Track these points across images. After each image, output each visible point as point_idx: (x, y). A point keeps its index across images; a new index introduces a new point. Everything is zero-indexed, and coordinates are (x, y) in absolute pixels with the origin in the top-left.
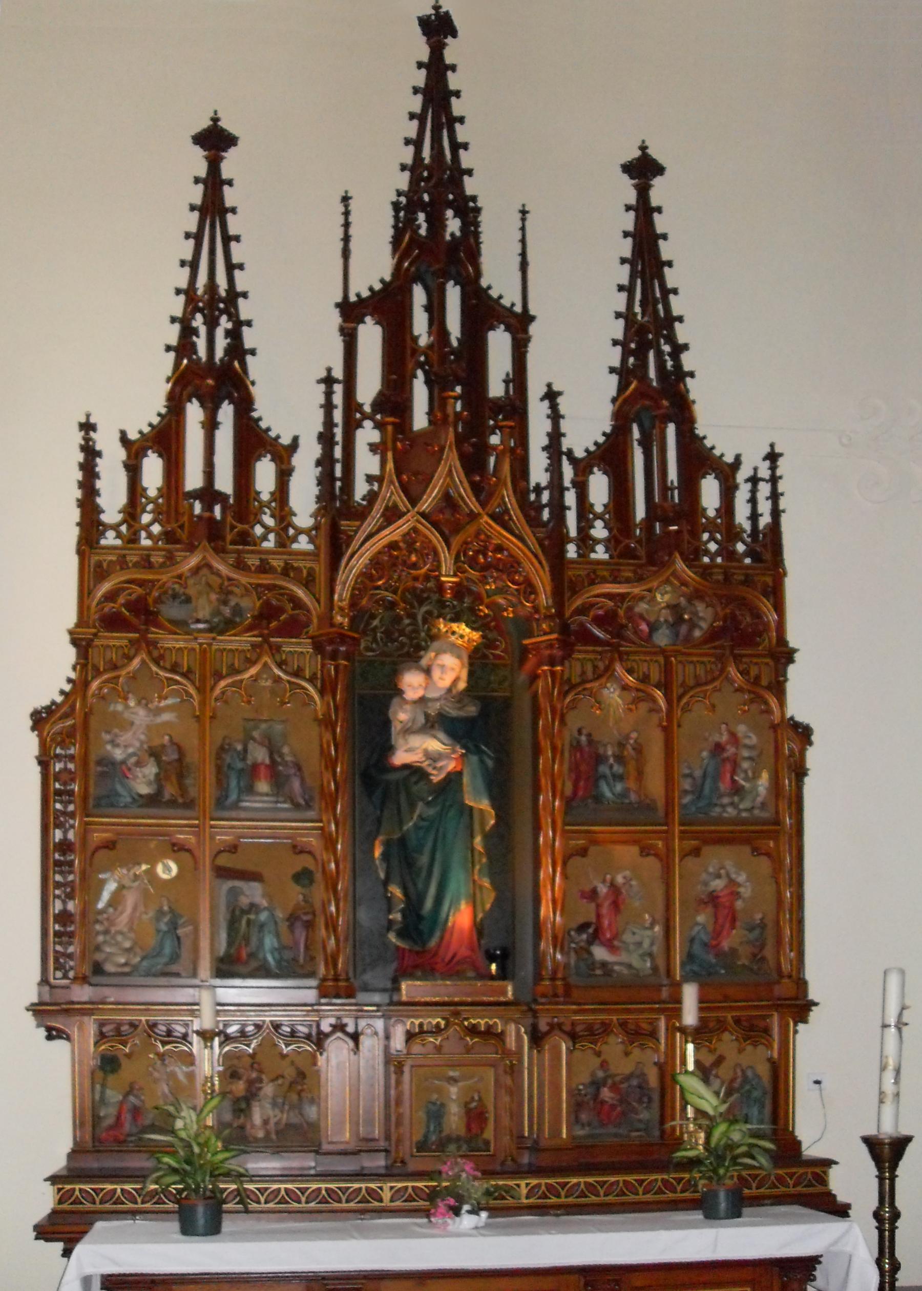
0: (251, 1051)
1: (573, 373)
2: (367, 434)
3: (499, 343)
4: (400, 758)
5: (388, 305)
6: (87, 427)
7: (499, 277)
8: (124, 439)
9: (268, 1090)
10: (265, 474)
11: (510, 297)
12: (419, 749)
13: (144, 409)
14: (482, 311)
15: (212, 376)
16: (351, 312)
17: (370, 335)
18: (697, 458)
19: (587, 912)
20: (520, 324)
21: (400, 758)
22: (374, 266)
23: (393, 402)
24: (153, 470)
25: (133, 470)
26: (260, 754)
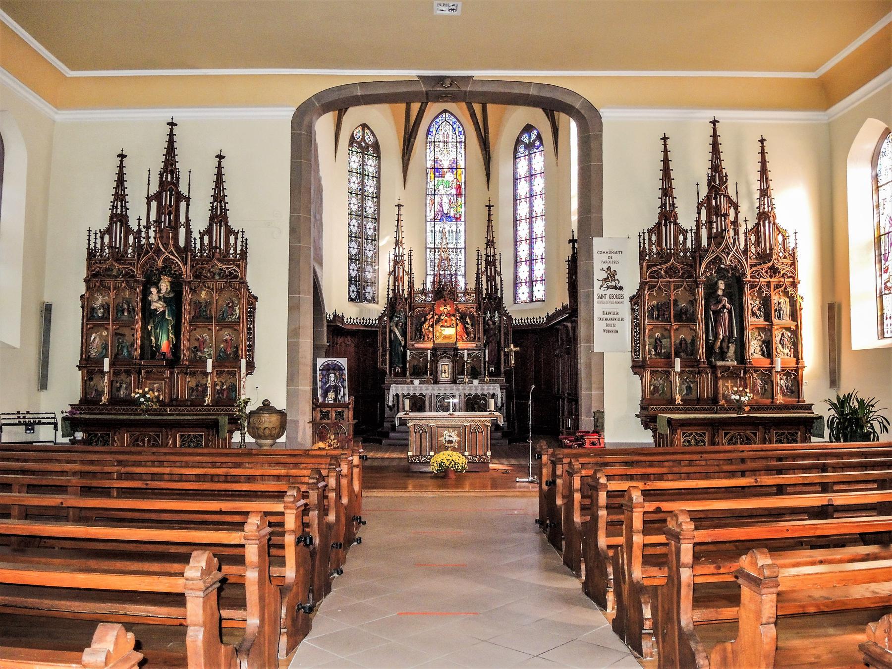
0: (496, 389)
1: (198, 215)
2: (153, 228)
3: (183, 204)
4: (152, 308)
5: (158, 197)
6: (90, 231)
7: (183, 189)
8: (200, 232)
9: (124, 386)
10: (232, 239)
11: (186, 193)
12: (158, 306)
13: (104, 224)
14: (179, 197)
15: (667, 215)
16: (149, 200)
17: (154, 204)
18: (229, 231)
19: (197, 344)
20: (188, 199)
21: (152, 308)
22: (154, 189)
23: (158, 222)
24: (206, 239)
25: (202, 239)
26: (125, 306)
